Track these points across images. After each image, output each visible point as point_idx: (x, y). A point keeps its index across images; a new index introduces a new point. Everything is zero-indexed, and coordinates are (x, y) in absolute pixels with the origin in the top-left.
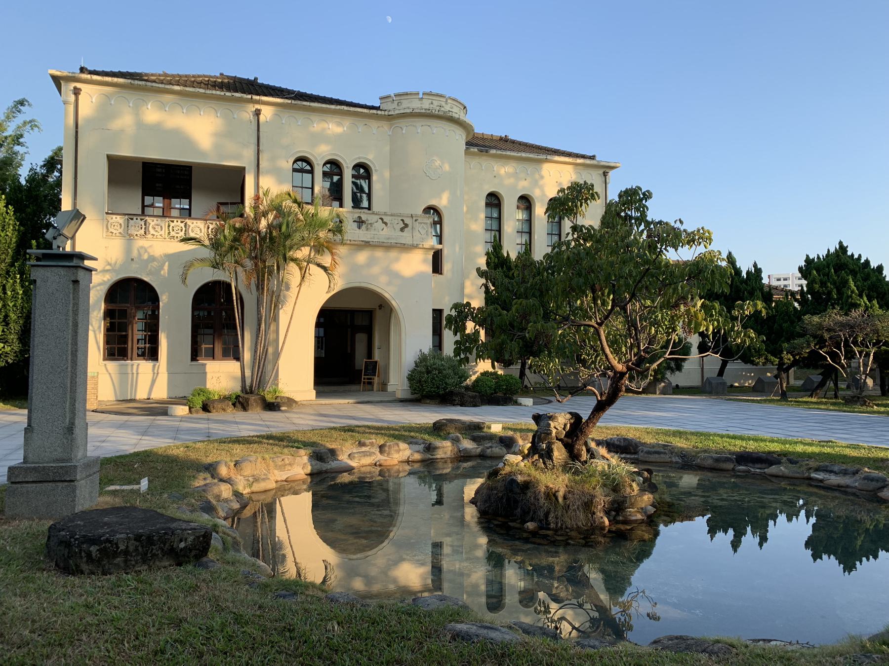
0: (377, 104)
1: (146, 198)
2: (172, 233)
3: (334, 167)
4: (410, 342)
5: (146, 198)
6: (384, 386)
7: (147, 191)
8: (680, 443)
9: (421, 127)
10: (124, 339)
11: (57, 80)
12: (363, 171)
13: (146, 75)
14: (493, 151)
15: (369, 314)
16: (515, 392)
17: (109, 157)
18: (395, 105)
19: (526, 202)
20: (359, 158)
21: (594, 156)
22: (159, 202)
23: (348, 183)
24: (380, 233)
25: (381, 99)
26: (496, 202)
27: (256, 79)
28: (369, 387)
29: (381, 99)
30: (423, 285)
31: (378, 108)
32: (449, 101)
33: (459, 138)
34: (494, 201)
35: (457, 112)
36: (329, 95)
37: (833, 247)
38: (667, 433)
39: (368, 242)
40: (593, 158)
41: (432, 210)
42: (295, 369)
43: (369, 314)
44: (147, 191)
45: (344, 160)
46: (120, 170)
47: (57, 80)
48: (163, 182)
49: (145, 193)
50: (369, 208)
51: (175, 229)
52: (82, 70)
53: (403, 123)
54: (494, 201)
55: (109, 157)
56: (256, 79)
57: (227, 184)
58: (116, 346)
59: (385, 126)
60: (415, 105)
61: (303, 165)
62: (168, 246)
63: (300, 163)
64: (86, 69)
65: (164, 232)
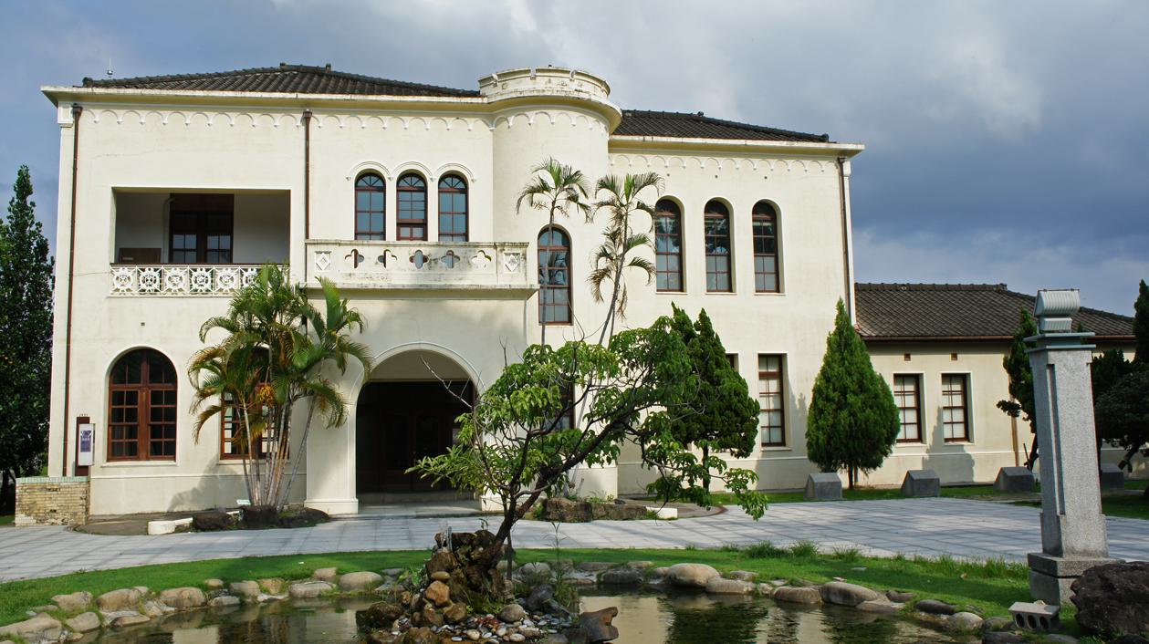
1: (175, 236)
2: (195, 286)
3: (412, 181)
5: (175, 236)
8: (1008, 561)
12: (455, 183)
20: (449, 165)
22: (191, 241)
26: (461, 186)
27: (329, 66)
28: (418, 232)
32: (575, 76)
36: (433, 84)
40: (823, 139)
45: (428, 171)
50: (783, 443)
51: (199, 279)
52: (88, 82)
56: (329, 66)
57: (269, 214)
59: (476, 126)
63: (448, 180)
64: (91, 80)
65: (184, 285)
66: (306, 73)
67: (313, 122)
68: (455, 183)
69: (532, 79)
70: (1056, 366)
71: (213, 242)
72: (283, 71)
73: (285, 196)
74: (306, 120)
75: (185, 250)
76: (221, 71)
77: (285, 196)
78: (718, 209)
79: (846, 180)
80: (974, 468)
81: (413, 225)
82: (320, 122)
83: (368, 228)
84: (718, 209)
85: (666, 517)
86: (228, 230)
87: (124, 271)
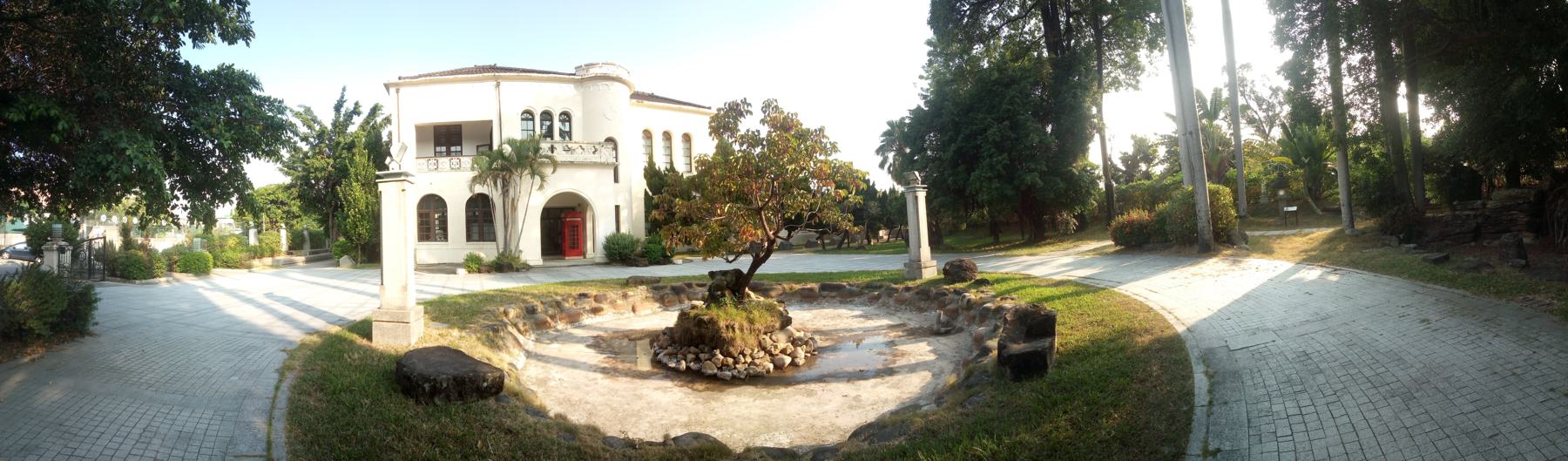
3: (547, 115)
4: (600, 229)
6: (583, 254)
7: (437, 144)
10: (428, 230)
11: (387, 86)
12: (566, 117)
19: (667, 136)
23: (553, 125)
24: (578, 156)
30: (616, 204)
33: (619, 93)
34: (648, 135)
35: (624, 76)
37: (817, 127)
41: (610, 140)
42: (530, 244)
44: (437, 144)
47: (387, 86)
48: (446, 138)
53: (590, 84)
54: (648, 135)
60: (593, 72)
61: (528, 115)
62: (454, 181)
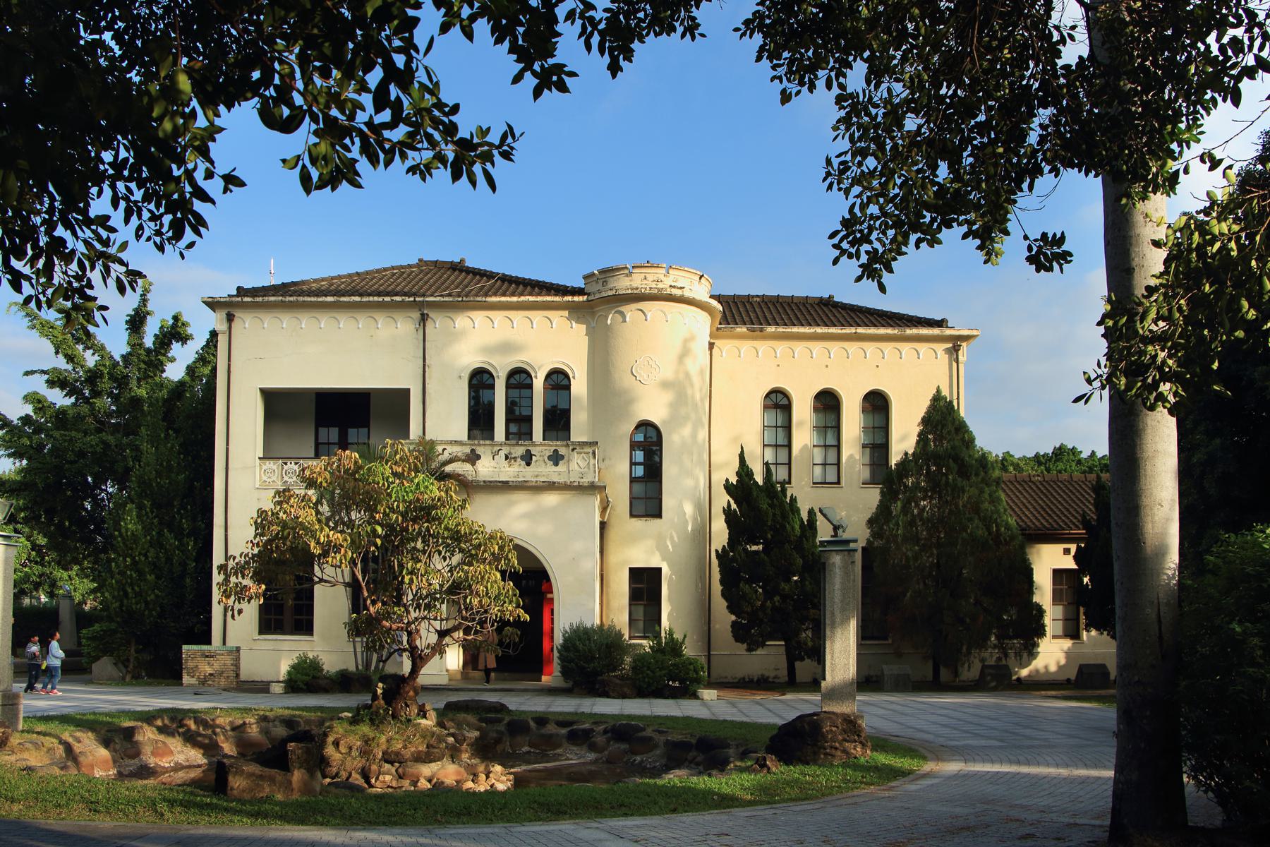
0: (580, 284)
3: (519, 379)
9: (652, 307)
13: (294, 284)
14: (771, 329)
15: (1157, 555)
16: (698, 681)
17: (262, 390)
18: (599, 287)
21: (943, 320)
22: (333, 434)
25: (585, 278)
27: (462, 261)
29: (585, 278)
31: (580, 292)
34: (778, 402)
38: (293, 709)
39: (507, 482)
40: (940, 324)
43: (1157, 555)
46: (280, 407)
49: (318, 425)
55: (262, 390)
56: (462, 261)
58: (273, 617)
66: (440, 268)
67: (429, 324)
68: (559, 380)
69: (627, 275)
70: (657, 521)
71: (352, 433)
72: (418, 266)
73: (405, 393)
74: (424, 319)
75: (329, 444)
76: (361, 270)
77: (405, 393)
78: (828, 402)
79: (961, 366)
80: (726, 604)
81: (519, 423)
82: (438, 322)
83: (480, 420)
84: (828, 402)
85: (37, 375)
86: (365, 423)
87: (271, 465)
